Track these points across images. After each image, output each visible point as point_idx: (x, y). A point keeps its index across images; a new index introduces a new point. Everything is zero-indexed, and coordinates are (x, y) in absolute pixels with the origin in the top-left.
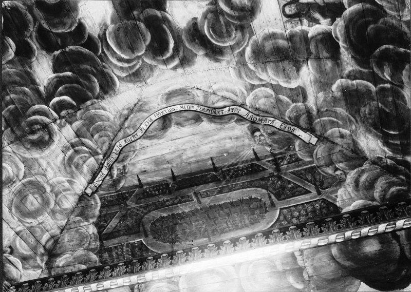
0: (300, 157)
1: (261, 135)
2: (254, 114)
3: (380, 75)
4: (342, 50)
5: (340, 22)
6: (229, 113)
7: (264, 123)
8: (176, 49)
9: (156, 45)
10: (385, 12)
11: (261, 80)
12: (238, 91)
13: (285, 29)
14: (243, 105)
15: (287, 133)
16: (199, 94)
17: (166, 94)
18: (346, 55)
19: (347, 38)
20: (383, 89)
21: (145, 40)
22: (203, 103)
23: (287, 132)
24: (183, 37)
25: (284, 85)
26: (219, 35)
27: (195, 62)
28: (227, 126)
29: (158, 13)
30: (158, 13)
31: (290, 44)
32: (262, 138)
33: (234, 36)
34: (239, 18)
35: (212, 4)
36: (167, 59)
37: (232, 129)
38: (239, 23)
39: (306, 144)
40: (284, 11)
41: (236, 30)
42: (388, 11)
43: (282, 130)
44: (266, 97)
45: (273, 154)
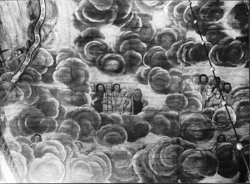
0: (3, 75)
1: (19, 55)
2: (34, 51)
3: (63, 123)
4: (77, 107)
5: (92, 109)
6: (36, 37)
7: (27, 56)
8: (88, 21)
9: (93, 10)
10: (97, 130)
11: (59, 62)
12: (52, 46)
13: (91, 83)
14: (40, 45)
15: (19, 68)
16: (51, 22)
17: (55, 3)
18: (74, 108)
19: (84, 111)
20: (54, 123)
21: (98, 5)
22: (45, 23)
23: (20, 68)
24: (94, 28)
25: (55, 73)
26: (91, 48)
27: (77, 29)
28: (26, 35)
29: (112, 20)
30: (112, 20)
31: (82, 83)
32: (17, 55)
33: (90, 56)
34: (99, 61)
35: (110, 50)
36: (82, 13)
37: (24, 38)
38: (97, 61)
39: (11, 77)
40: (100, 84)
41: (93, 58)
42: (98, 131)
43: (21, 65)
44: (46, 61)
45: (4, 61)
